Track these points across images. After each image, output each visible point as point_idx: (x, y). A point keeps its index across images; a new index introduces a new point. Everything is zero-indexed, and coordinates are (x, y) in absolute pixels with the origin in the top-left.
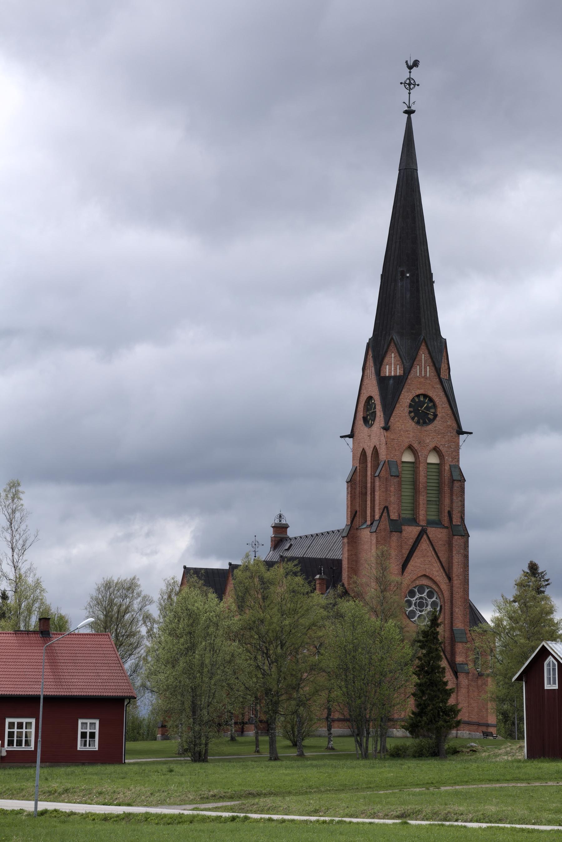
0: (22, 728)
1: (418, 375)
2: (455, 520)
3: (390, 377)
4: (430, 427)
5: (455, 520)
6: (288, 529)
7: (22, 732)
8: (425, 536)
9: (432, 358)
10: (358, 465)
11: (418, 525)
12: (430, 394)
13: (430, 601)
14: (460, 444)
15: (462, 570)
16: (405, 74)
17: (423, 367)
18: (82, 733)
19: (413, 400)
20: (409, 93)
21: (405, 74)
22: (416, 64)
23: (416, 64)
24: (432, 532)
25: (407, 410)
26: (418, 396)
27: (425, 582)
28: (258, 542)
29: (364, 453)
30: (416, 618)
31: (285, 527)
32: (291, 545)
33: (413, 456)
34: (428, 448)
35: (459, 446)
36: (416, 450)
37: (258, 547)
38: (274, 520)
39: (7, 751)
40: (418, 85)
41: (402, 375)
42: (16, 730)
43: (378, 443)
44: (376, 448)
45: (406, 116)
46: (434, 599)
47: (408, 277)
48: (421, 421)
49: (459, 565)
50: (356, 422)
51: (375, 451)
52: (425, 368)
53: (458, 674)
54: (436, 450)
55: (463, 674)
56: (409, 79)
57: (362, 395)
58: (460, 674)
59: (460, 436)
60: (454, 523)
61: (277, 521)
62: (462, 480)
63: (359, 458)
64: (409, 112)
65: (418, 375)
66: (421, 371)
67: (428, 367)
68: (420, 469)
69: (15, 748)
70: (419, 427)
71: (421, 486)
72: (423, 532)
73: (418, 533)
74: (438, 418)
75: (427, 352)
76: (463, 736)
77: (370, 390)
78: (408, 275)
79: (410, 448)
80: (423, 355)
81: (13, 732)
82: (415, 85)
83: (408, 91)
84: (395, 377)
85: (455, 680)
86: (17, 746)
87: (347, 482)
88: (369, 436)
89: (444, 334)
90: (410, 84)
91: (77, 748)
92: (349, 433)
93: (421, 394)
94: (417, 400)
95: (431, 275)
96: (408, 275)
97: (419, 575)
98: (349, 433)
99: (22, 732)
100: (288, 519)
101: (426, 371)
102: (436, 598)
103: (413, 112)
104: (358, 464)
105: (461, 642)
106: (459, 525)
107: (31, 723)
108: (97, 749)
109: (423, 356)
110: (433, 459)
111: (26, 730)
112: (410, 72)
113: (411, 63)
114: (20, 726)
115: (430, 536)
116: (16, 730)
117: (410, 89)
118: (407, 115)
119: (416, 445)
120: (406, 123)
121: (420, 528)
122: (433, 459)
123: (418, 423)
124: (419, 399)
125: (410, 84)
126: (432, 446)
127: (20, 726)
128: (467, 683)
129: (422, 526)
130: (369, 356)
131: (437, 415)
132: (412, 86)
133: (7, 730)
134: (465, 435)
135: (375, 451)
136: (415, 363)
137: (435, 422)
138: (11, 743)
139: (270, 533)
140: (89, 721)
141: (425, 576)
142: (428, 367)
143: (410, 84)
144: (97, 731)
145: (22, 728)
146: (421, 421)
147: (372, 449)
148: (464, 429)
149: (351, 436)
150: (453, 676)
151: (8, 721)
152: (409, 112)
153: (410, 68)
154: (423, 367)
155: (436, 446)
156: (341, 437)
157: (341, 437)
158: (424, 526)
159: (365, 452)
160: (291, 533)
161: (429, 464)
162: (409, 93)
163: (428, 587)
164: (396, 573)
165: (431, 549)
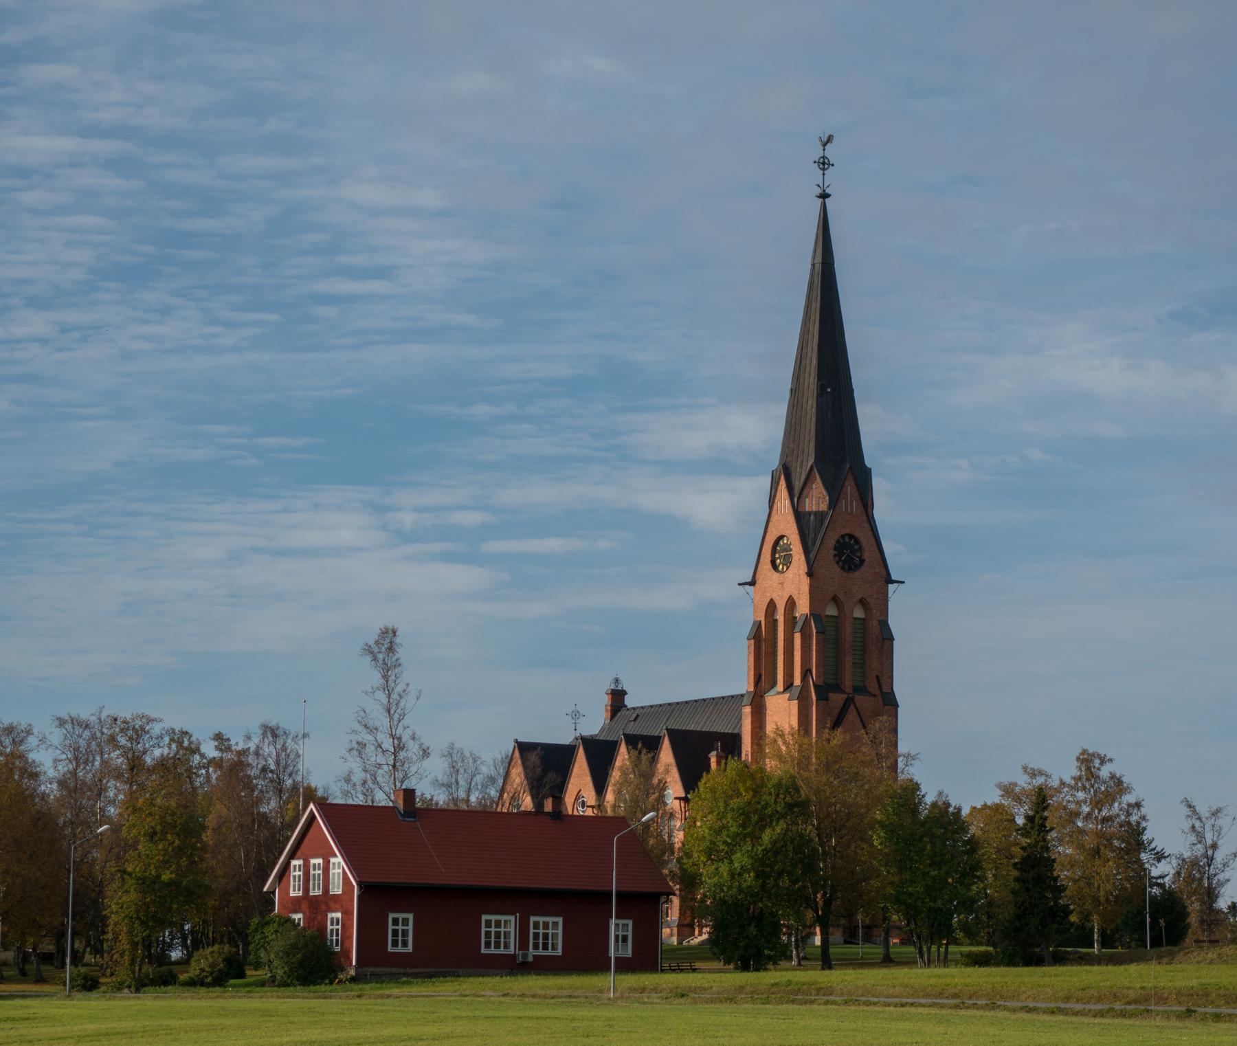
0: (491, 927)
1: (844, 510)
2: (885, 687)
3: (809, 513)
4: (857, 574)
5: (885, 687)
6: (626, 697)
7: (543, 929)
8: (852, 706)
9: (858, 489)
10: (762, 619)
11: (844, 692)
12: (857, 534)
14: (889, 596)
16: (831, 151)
18: (486, 932)
19: (838, 542)
20: (824, 174)
21: (831, 151)
22: (830, 139)
23: (830, 139)
24: (859, 699)
25: (833, 552)
26: (843, 536)
28: (578, 712)
29: (772, 606)
31: (622, 693)
32: (638, 716)
33: (836, 608)
35: (888, 597)
36: (841, 602)
37: (578, 718)
38: (608, 685)
39: (534, 956)
40: (833, 165)
41: (826, 510)
42: (493, 930)
43: (795, 593)
44: (793, 598)
45: (821, 200)
47: (832, 390)
48: (846, 567)
50: (759, 566)
51: (791, 604)
52: (852, 502)
54: (863, 602)
56: (824, 157)
57: (768, 534)
59: (890, 585)
60: (884, 691)
61: (613, 687)
62: (892, 639)
63: (764, 611)
65: (844, 510)
66: (846, 506)
67: (854, 502)
68: (846, 624)
69: (541, 952)
70: (845, 574)
71: (847, 646)
72: (849, 702)
73: (843, 702)
74: (865, 564)
75: (853, 483)
77: (782, 527)
78: (829, 390)
79: (835, 599)
81: (539, 933)
82: (829, 164)
83: (822, 172)
84: (816, 513)
86: (495, 948)
88: (782, 584)
89: (868, 463)
90: (824, 164)
91: (480, 951)
92: (749, 579)
93: (847, 534)
94: (842, 541)
95: (853, 390)
96: (829, 390)
98: (750, 580)
99: (543, 929)
100: (625, 685)
101: (852, 506)
103: (828, 196)
104: (764, 618)
107: (557, 923)
108: (411, 951)
109: (850, 488)
110: (859, 613)
111: (553, 931)
112: (824, 150)
113: (825, 139)
114: (498, 924)
115: (857, 706)
116: (493, 930)
117: (824, 169)
118: (821, 200)
119: (842, 597)
121: (846, 696)
122: (859, 613)
123: (843, 568)
124: (844, 540)
125: (824, 163)
126: (859, 596)
127: (498, 924)
129: (848, 694)
130: (780, 486)
131: (864, 560)
132: (826, 166)
133: (484, 929)
135: (791, 604)
137: (863, 568)
138: (536, 947)
139: (606, 700)
140: (401, 916)
142: (854, 502)
143: (824, 164)
144: (630, 934)
145: (491, 927)
146: (846, 567)
147: (786, 600)
148: (894, 578)
149: (753, 583)
151: (391, 916)
152: (824, 196)
153: (825, 145)
155: (863, 598)
156: (740, 584)
157: (740, 584)
158: (850, 693)
159: (775, 607)
160: (630, 702)
161: (855, 618)
162: (824, 174)
165: (859, 721)
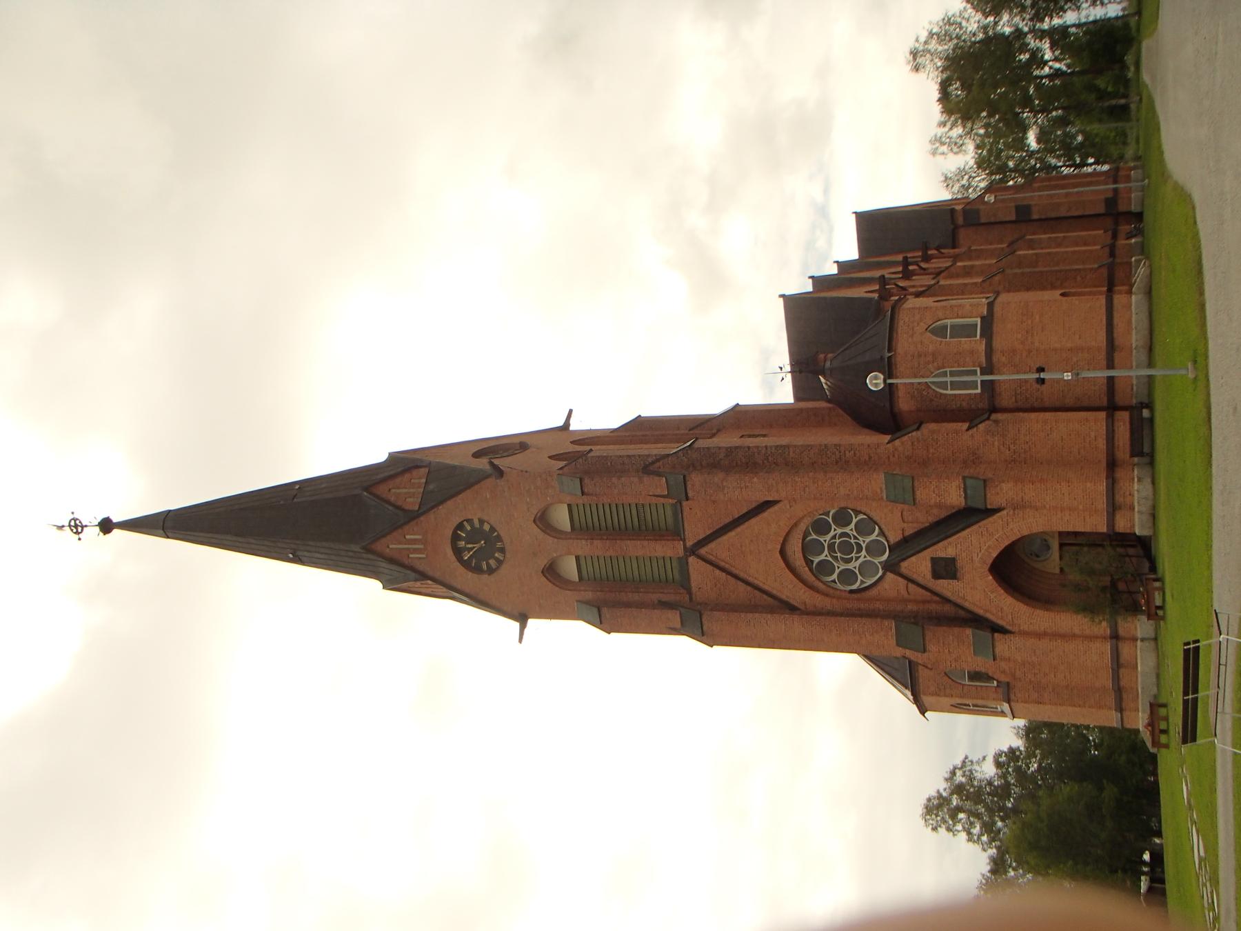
13: (864, 541)
15: (755, 479)
17: (410, 546)
27: (795, 548)
30: (835, 576)
34: (541, 535)
46: (873, 537)
49: (746, 487)
53: (989, 507)
55: (988, 496)
58: (988, 502)
64: (106, 526)
65: (424, 556)
66: (416, 551)
67: (408, 537)
75: (384, 541)
76: (1146, 498)
80: (391, 546)
85: (1005, 512)
87: (1014, 717)
97: (783, 565)
102: (812, 562)
105: (913, 491)
106: (666, 479)
120: (547, 621)
128: (1010, 485)
134: (572, 421)
136: (406, 563)
141: (782, 552)
142: (408, 537)
146: (499, 545)
148: (560, 423)
150: (995, 517)
154: (410, 546)
163: (806, 534)
164: (783, 627)
